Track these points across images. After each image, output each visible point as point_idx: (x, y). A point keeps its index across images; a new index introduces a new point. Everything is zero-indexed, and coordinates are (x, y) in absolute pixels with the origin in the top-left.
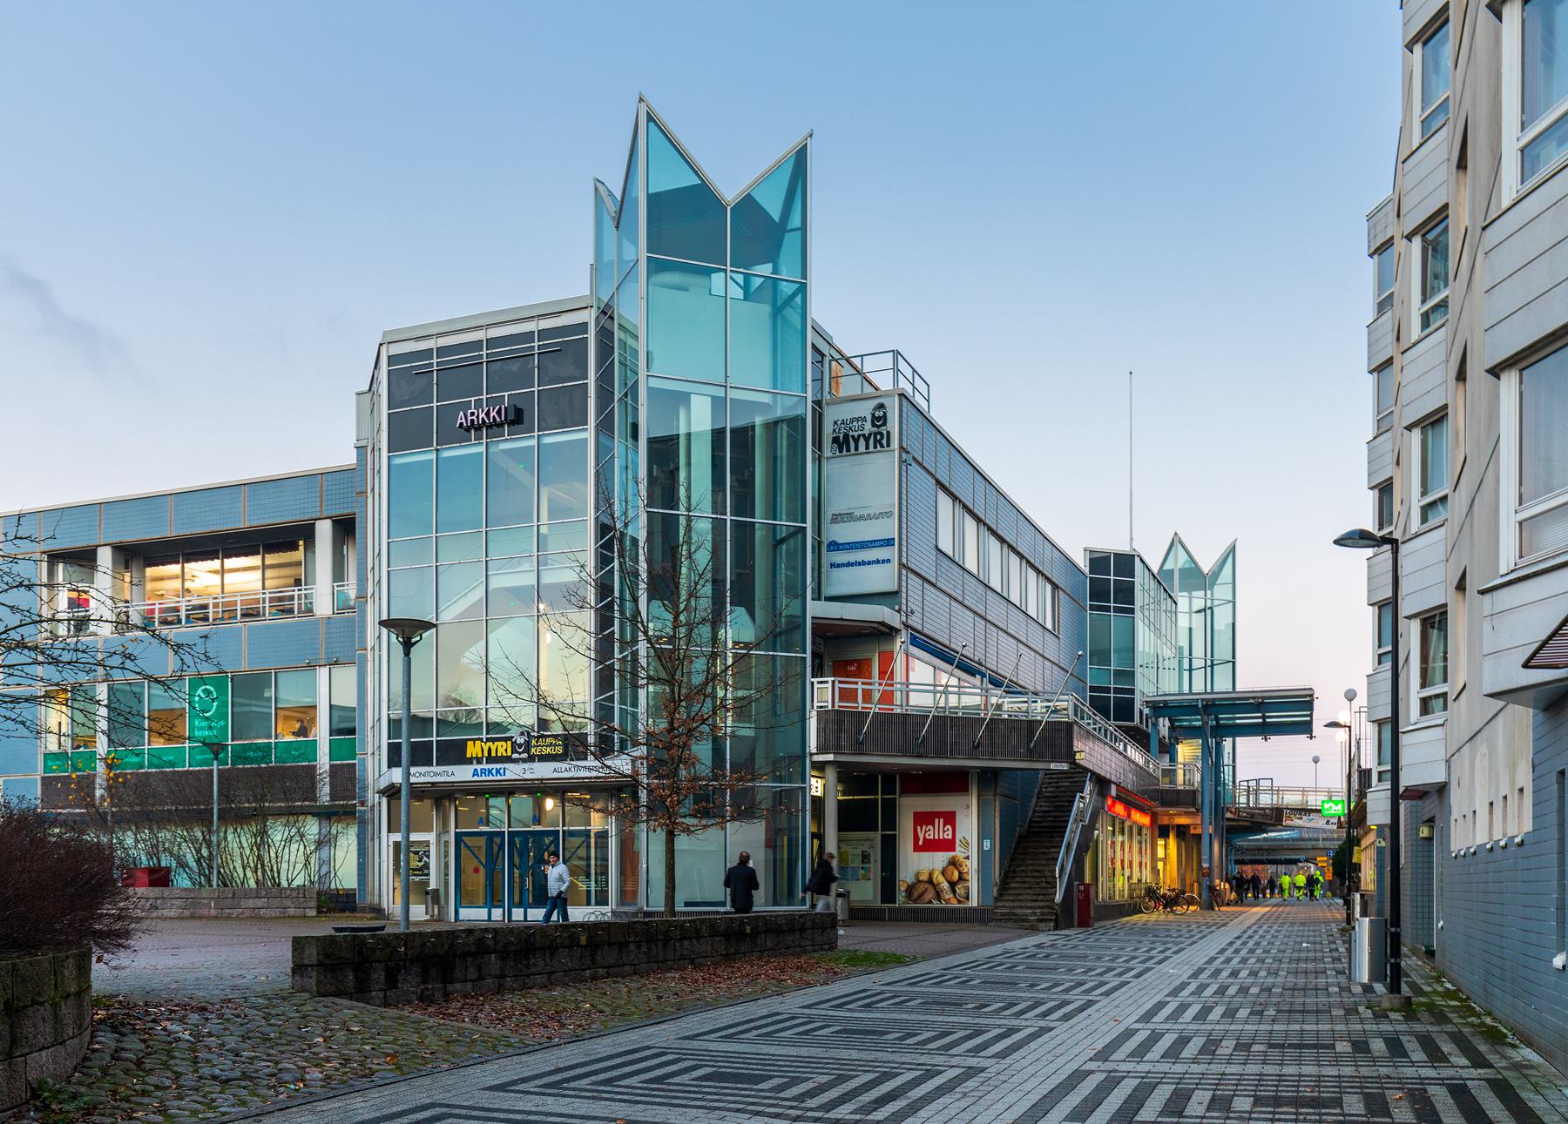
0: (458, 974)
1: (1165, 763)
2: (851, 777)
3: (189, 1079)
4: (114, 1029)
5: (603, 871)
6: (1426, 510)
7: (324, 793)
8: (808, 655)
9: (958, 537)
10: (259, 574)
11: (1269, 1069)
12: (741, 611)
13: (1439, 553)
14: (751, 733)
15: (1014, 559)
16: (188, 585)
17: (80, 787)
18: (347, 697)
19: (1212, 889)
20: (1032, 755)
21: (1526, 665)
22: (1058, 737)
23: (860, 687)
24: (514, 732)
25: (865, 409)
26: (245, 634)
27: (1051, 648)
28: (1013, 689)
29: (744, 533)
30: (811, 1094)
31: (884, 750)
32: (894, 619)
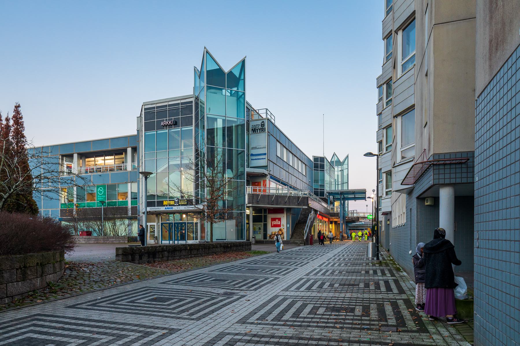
0: (157, 256)
1: (332, 206)
2: (256, 210)
3: (87, 282)
4: (70, 270)
5: (197, 232)
6: (387, 148)
7: (130, 213)
8: (246, 181)
9: (282, 153)
10: (113, 161)
11: (345, 277)
12: (229, 170)
13: (390, 158)
14: (232, 199)
15: (296, 158)
16: (96, 163)
17: (69, 212)
18: (135, 190)
19: (342, 236)
20: (299, 204)
21: (401, 184)
22: (305, 200)
23: (258, 188)
24: (175, 199)
25: (259, 123)
26: (110, 175)
27: (305, 179)
28: (294, 189)
29: (230, 152)
30: (237, 284)
31: (264, 204)
32: (266, 172)
